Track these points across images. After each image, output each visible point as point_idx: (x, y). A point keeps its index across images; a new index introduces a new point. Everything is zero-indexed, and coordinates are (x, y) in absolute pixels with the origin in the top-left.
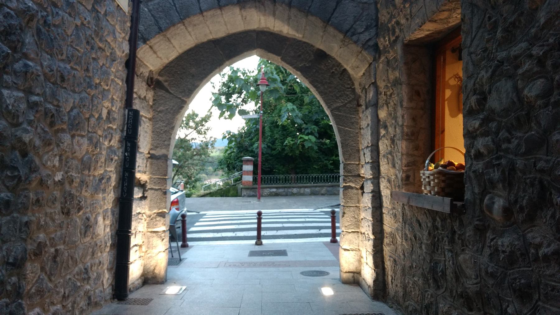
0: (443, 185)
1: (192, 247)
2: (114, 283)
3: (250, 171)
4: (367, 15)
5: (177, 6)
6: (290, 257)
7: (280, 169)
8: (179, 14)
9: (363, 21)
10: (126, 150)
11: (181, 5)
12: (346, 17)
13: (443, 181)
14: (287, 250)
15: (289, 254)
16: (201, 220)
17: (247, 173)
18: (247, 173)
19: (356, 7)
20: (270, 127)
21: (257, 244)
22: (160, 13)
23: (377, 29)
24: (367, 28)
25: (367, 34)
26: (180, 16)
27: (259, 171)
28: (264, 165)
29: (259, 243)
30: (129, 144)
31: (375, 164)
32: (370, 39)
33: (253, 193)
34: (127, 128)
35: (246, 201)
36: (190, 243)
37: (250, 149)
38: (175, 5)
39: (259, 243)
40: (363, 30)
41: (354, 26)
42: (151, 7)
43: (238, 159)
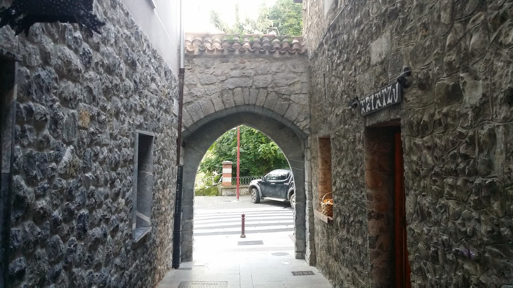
0: (328, 210)
3: (229, 174)
4: (305, 112)
6: (265, 245)
7: (256, 170)
10: (177, 188)
13: (329, 208)
17: (227, 175)
18: (227, 175)
20: (246, 135)
23: (310, 120)
24: (305, 119)
25: (305, 122)
27: (238, 174)
28: (242, 167)
30: (179, 185)
31: (310, 193)
33: (233, 193)
37: (229, 154)
38: (201, 108)
39: (243, 236)
42: (188, 109)
43: (218, 162)
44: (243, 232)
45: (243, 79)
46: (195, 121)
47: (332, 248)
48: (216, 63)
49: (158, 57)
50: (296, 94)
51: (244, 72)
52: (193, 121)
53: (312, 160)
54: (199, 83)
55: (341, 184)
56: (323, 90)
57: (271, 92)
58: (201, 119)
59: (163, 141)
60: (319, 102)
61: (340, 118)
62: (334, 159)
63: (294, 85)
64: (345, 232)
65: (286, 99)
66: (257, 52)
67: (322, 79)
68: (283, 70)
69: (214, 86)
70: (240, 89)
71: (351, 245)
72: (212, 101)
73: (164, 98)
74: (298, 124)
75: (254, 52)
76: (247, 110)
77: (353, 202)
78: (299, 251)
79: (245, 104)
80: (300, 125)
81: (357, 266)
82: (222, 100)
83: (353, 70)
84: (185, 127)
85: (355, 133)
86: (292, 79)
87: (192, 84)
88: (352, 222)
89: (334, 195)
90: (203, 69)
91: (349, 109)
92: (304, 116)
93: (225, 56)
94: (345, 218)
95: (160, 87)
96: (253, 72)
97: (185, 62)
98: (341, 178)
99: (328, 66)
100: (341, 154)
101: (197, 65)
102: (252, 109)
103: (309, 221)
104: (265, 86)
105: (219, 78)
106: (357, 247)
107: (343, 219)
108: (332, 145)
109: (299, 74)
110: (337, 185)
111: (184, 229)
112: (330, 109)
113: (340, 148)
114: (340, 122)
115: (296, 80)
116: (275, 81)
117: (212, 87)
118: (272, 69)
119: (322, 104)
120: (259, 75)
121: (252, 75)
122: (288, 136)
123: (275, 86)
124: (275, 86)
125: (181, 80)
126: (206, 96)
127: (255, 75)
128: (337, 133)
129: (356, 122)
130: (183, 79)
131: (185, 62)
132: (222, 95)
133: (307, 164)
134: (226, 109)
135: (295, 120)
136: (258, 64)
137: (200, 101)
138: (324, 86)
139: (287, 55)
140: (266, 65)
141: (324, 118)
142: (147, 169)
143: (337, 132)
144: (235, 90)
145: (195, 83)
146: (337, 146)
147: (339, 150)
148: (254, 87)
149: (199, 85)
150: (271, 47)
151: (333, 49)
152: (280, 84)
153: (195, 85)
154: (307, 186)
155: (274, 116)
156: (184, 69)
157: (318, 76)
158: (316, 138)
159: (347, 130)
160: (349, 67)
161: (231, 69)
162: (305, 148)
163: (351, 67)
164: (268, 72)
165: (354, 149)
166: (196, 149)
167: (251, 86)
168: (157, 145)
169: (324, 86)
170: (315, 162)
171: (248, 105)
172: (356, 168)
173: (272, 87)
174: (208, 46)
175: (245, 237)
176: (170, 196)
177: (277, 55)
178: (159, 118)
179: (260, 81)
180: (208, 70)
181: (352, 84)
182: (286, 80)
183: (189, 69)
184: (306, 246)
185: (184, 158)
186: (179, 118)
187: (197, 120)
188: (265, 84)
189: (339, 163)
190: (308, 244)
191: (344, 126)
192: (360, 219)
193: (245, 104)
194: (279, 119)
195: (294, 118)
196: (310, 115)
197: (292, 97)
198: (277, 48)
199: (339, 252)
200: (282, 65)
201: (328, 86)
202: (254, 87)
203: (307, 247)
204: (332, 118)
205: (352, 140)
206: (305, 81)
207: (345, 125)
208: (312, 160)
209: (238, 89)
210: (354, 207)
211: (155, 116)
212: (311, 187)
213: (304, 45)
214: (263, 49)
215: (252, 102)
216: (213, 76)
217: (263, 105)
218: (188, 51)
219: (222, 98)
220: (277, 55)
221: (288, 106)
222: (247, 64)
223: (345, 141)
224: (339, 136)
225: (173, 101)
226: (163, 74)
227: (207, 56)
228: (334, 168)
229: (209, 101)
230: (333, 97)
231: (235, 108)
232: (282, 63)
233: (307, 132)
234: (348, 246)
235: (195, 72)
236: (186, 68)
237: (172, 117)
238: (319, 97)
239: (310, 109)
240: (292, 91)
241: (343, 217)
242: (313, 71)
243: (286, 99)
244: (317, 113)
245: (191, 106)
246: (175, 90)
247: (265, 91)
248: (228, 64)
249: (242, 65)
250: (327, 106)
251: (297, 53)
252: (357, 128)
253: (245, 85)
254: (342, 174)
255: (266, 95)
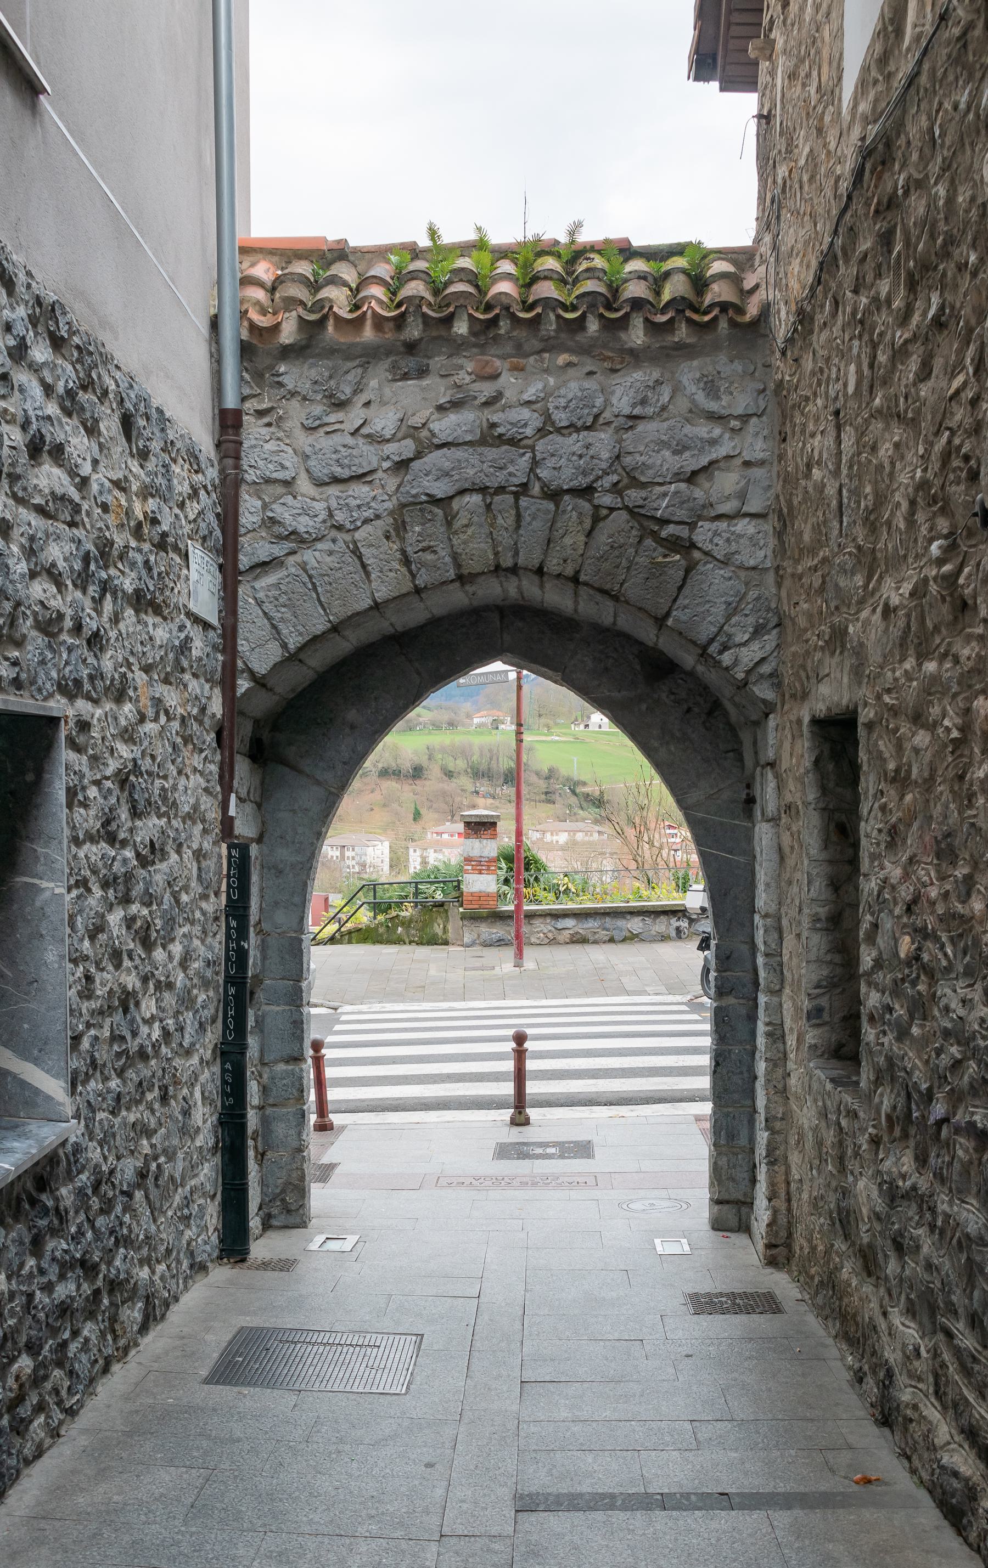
1: (343, 1128)
2: (220, 1227)
5: (319, 589)
6: (599, 1163)
8: (325, 610)
9: (746, 615)
11: (329, 588)
12: (707, 606)
14: (595, 1141)
15: (597, 1151)
16: (338, 1027)
19: (730, 579)
21: (514, 1122)
22: (283, 610)
23: (780, 635)
24: (758, 631)
25: (755, 646)
26: (327, 614)
29: (520, 1120)
32: (763, 660)
34: (229, 886)
35: (478, 963)
36: (336, 1119)
40: (746, 637)
41: (725, 628)
42: (261, 595)
44: (520, 1102)
45: (491, 453)
46: (292, 647)
47: (853, 1215)
48: (374, 383)
49: (76, 340)
50: (719, 517)
51: (495, 418)
52: (284, 646)
53: (784, 819)
54: (303, 476)
55: (896, 940)
56: (831, 490)
57: (612, 510)
58: (315, 639)
59: (128, 736)
60: (813, 552)
61: (901, 623)
62: (872, 822)
63: (710, 478)
64: (907, 1163)
65: (674, 544)
66: (550, 325)
67: (830, 441)
68: (664, 408)
69: (366, 489)
70: (476, 499)
71: (932, 1227)
72: (360, 557)
73: (119, 539)
74: (727, 658)
75: (537, 321)
76: (513, 591)
77: (947, 1033)
78: (726, 1197)
79: (498, 567)
80: (736, 662)
81: (959, 1327)
82: (403, 552)
83: (971, 371)
84: (252, 675)
85: (970, 700)
86: (701, 450)
87: (276, 481)
88: (940, 1123)
89: (869, 984)
90: (318, 409)
91: (945, 577)
92: (751, 620)
93: (411, 348)
94: (909, 1096)
95: (95, 487)
96: (530, 419)
97: (242, 378)
98: (897, 911)
99: (852, 368)
100: (902, 798)
101: (293, 394)
102: (530, 589)
103: (768, 1081)
104: (584, 481)
105: (390, 448)
106: (959, 1242)
107: (901, 1101)
108: (863, 756)
109: (734, 423)
110: (879, 941)
111: (271, 1101)
112: (859, 580)
113: (897, 771)
114: (903, 643)
115: (722, 451)
116: (627, 460)
117: (361, 491)
118: (614, 401)
119: (825, 560)
120: (559, 430)
121: (529, 431)
122: (689, 710)
123: (626, 481)
124: (626, 481)
125: (230, 462)
126: (334, 533)
127: (542, 432)
128: (887, 699)
129: (974, 644)
130: (238, 458)
131: (242, 378)
132: (400, 527)
133: (764, 835)
134: (418, 591)
135: (712, 640)
136: (551, 381)
137: (308, 556)
138: (836, 473)
139: (682, 333)
140: (591, 384)
141: (832, 627)
142: (40, 868)
143: (889, 691)
144: (455, 505)
145: (285, 475)
146: (885, 760)
147: (894, 780)
148: (536, 489)
149: (304, 485)
150: (611, 298)
151: (879, 276)
152: (651, 472)
153: (287, 483)
154: (761, 932)
155: (625, 622)
156: (238, 413)
157: (811, 427)
158: (799, 722)
159: (933, 686)
160: (947, 358)
161: (441, 408)
162: (757, 763)
163: (961, 352)
164: (597, 417)
165: (961, 778)
166: (307, 770)
167: (525, 486)
168: (94, 759)
169: (836, 473)
170: (794, 829)
171: (514, 570)
172: (966, 871)
173: (616, 489)
174: (338, 297)
175: (527, 1122)
176: (191, 972)
177: (637, 335)
178: (96, 635)
179: (563, 462)
180: (340, 415)
181: (961, 446)
182: (675, 452)
183: (260, 413)
184: (754, 1181)
185: (259, 806)
186: (223, 636)
187: (301, 640)
188: (584, 473)
189: (894, 836)
190: (762, 1174)
191: (920, 665)
192: (977, 1118)
193: (498, 567)
194: (647, 633)
195: (705, 631)
196: (777, 612)
197: (703, 534)
198: (637, 304)
199: (879, 1241)
200: (658, 383)
201: (851, 467)
202: (536, 489)
203: (758, 1185)
204: (867, 623)
205: (955, 734)
206: (761, 455)
207: (922, 657)
208: (784, 819)
209: (467, 498)
210: (953, 1057)
211: (68, 623)
212: (776, 936)
213: (757, 286)
214: (574, 308)
215: (529, 556)
216: (361, 441)
217: (577, 572)
218: (253, 327)
219: (403, 539)
220: (637, 335)
221: (682, 573)
222: (508, 381)
223: (922, 738)
224: (894, 711)
225: (186, 557)
226: (110, 426)
227: (332, 352)
228: (872, 862)
229: (349, 558)
230: (872, 526)
231: (457, 584)
232: (656, 374)
233: (764, 691)
234: (919, 1225)
235: (287, 425)
236: (250, 405)
237: (182, 628)
238: (816, 529)
239: (779, 585)
240: (704, 506)
241: (903, 1093)
242: (793, 407)
243: (674, 544)
244: (806, 606)
245: (271, 579)
246: (193, 509)
247: (585, 506)
248: (425, 382)
249: (486, 390)
250: (849, 566)
251: (723, 324)
252: (980, 672)
253: (500, 478)
254: (906, 893)
255: (588, 523)
